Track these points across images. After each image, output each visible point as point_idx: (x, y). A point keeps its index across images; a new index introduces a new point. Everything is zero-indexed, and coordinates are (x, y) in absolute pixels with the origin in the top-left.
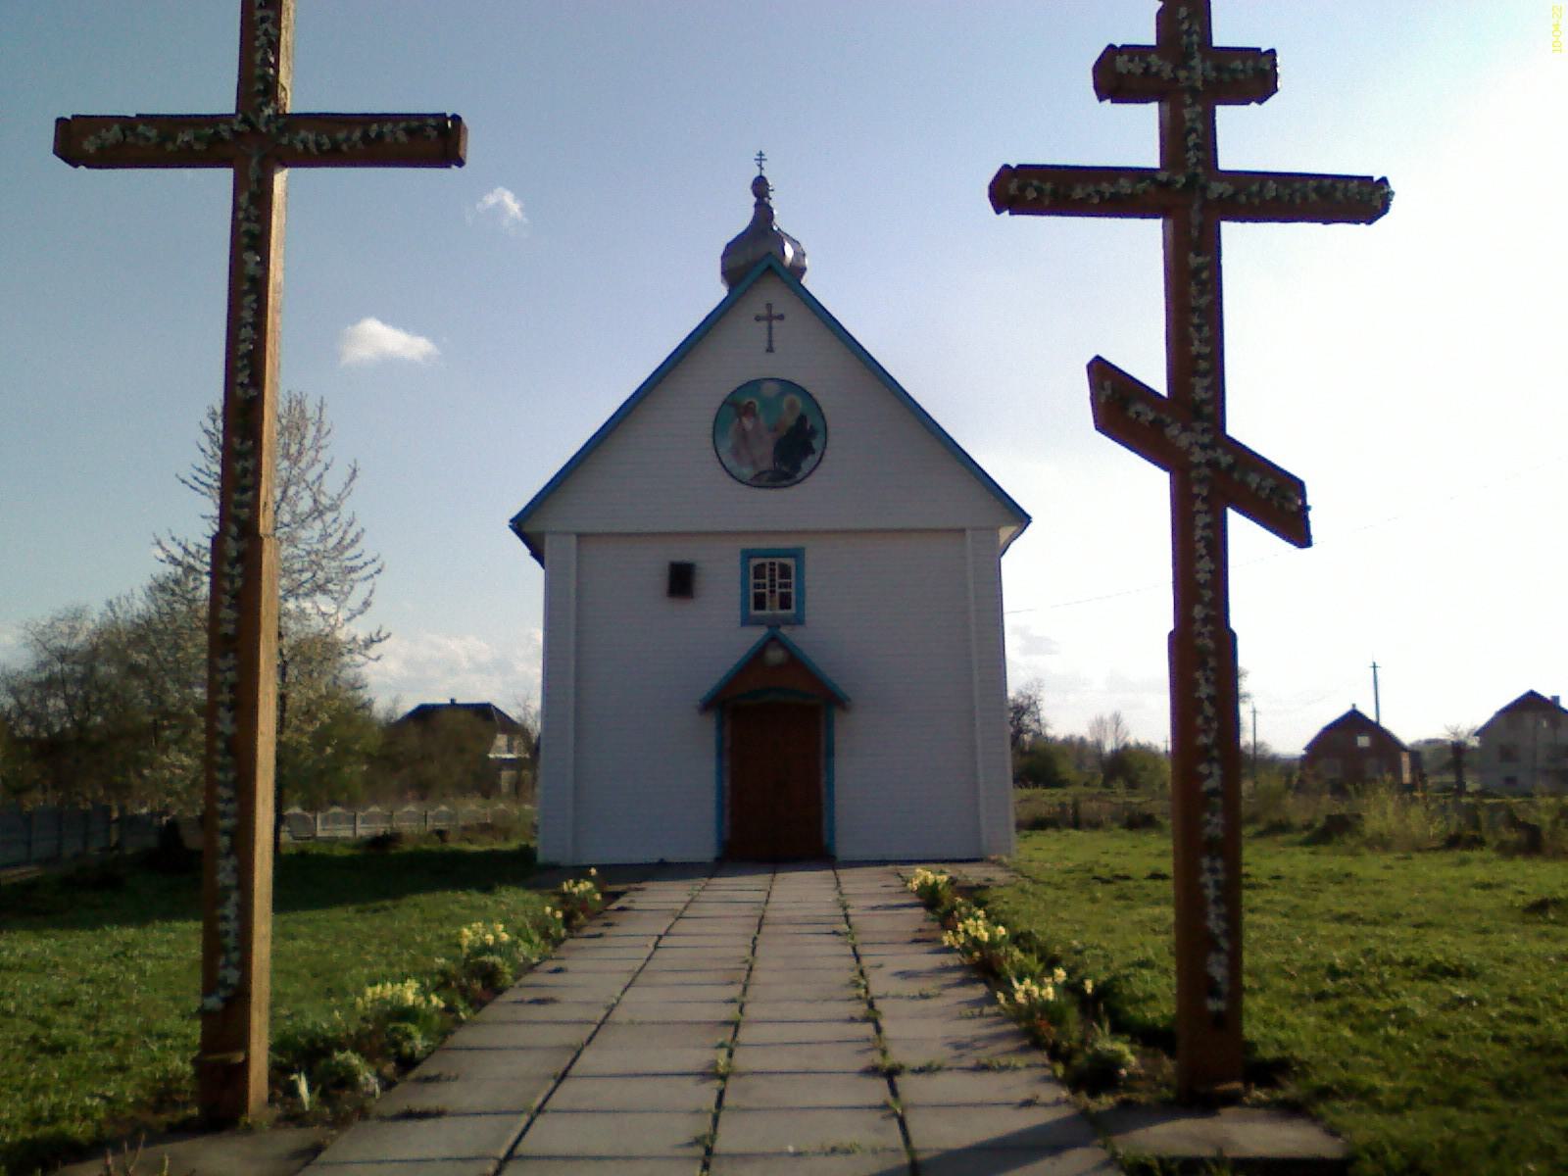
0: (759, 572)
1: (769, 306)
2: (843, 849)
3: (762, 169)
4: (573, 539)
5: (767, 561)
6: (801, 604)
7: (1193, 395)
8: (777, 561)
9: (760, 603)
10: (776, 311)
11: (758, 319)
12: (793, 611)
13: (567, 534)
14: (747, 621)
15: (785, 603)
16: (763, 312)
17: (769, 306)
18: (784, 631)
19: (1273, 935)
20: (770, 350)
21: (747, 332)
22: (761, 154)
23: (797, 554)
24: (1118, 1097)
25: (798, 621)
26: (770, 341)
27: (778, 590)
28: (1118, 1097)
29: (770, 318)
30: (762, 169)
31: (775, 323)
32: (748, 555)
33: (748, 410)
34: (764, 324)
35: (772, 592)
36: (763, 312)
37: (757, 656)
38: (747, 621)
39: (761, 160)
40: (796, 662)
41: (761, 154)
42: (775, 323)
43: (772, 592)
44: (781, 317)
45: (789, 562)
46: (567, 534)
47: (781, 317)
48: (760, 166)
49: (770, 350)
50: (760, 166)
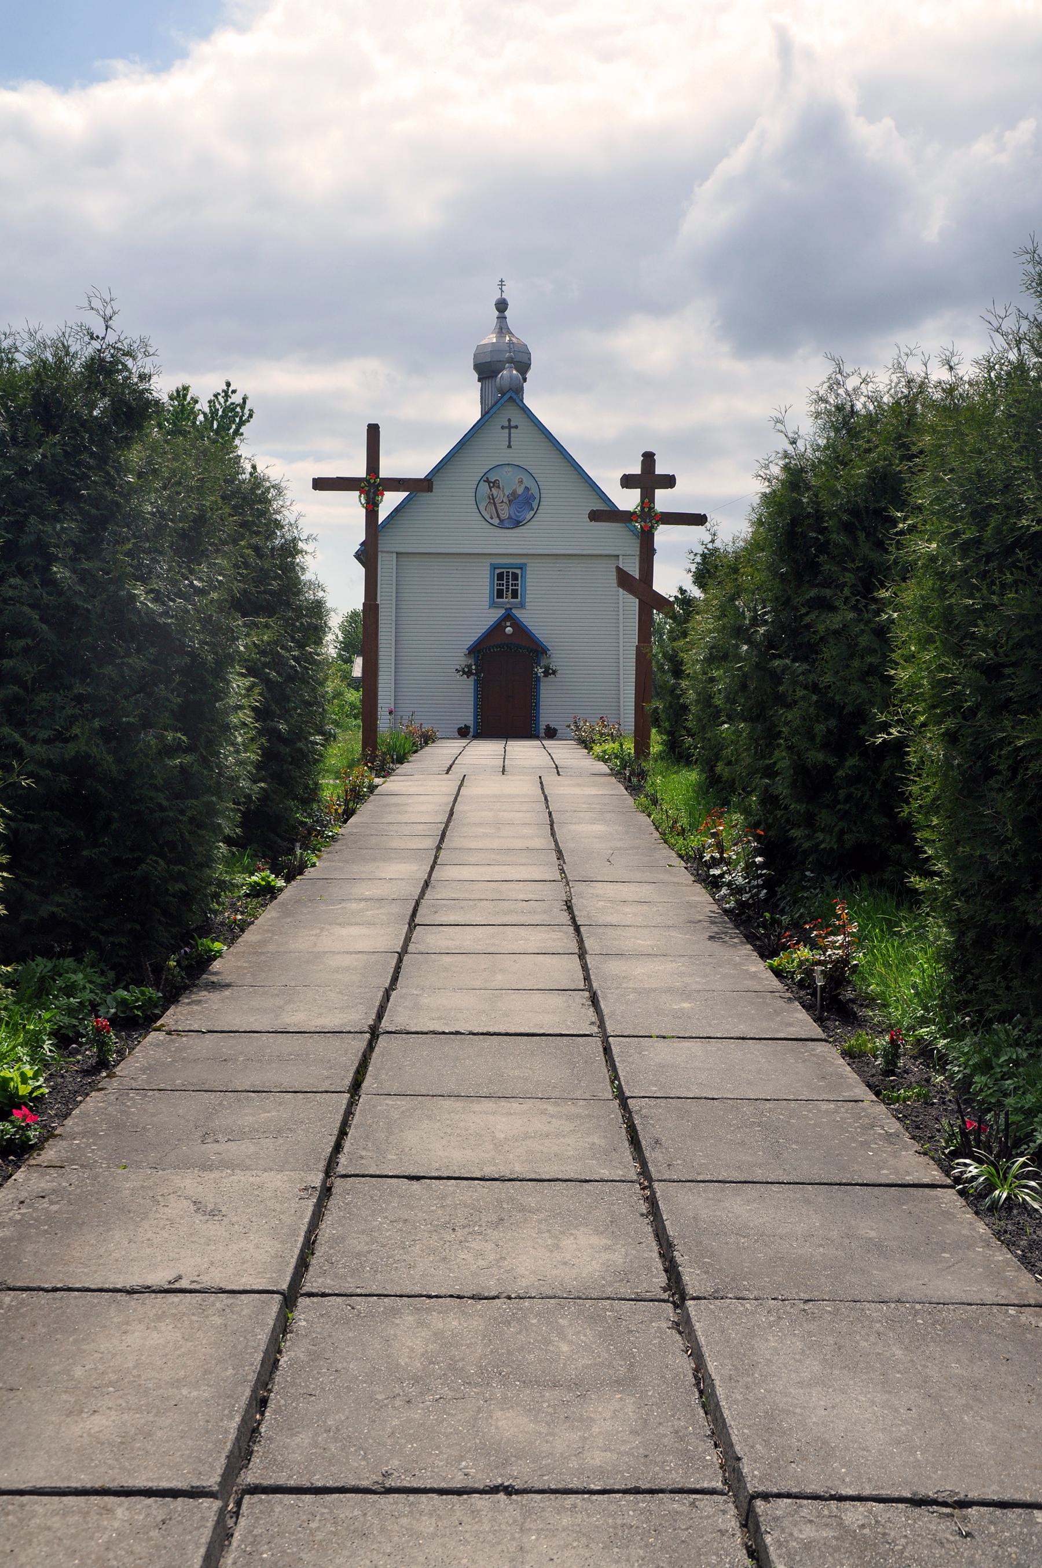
0: (500, 576)
1: (509, 420)
2: (546, 718)
3: (502, 291)
4: (395, 555)
5: (505, 570)
6: (523, 596)
7: (683, 764)
8: (511, 571)
9: (500, 595)
10: (513, 424)
11: (503, 428)
12: (519, 600)
13: (392, 552)
14: (493, 605)
15: (515, 594)
16: (506, 424)
17: (509, 420)
18: (514, 611)
19: (362, 1519)
20: (509, 446)
21: (497, 436)
22: (502, 281)
23: (521, 567)
24: (853, 520)
25: (522, 605)
26: (510, 442)
27: (511, 588)
28: (853, 520)
29: (510, 427)
30: (502, 291)
31: (513, 431)
32: (494, 567)
33: (494, 484)
34: (507, 431)
35: (507, 588)
36: (506, 424)
37: (497, 627)
38: (493, 605)
39: (502, 285)
40: (521, 629)
41: (502, 281)
42: (513, 431)
43: (507, 588)
44: (516, 427)
45: (518, 571)
46: (392, 552)
47: (516, 427)
48: (501, 289)
49: (509, 446)
50: (501, 289)
